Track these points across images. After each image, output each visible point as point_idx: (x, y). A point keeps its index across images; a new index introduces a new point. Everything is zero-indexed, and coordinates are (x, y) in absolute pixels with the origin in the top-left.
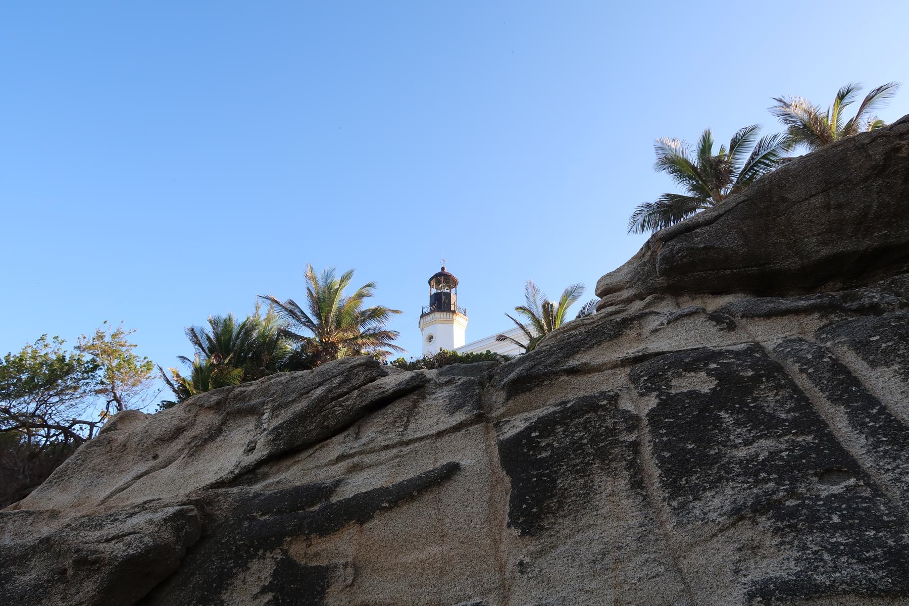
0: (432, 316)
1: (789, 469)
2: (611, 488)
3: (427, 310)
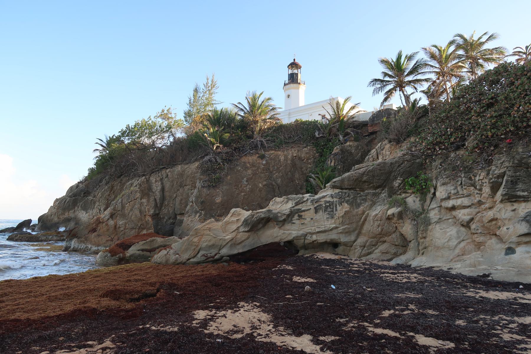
0: (289, 86)
1: (330, 212)
2: (321, 211)
3: (287, 82)
